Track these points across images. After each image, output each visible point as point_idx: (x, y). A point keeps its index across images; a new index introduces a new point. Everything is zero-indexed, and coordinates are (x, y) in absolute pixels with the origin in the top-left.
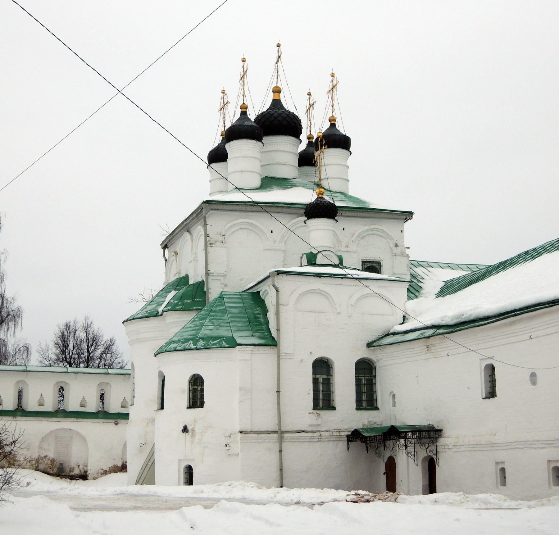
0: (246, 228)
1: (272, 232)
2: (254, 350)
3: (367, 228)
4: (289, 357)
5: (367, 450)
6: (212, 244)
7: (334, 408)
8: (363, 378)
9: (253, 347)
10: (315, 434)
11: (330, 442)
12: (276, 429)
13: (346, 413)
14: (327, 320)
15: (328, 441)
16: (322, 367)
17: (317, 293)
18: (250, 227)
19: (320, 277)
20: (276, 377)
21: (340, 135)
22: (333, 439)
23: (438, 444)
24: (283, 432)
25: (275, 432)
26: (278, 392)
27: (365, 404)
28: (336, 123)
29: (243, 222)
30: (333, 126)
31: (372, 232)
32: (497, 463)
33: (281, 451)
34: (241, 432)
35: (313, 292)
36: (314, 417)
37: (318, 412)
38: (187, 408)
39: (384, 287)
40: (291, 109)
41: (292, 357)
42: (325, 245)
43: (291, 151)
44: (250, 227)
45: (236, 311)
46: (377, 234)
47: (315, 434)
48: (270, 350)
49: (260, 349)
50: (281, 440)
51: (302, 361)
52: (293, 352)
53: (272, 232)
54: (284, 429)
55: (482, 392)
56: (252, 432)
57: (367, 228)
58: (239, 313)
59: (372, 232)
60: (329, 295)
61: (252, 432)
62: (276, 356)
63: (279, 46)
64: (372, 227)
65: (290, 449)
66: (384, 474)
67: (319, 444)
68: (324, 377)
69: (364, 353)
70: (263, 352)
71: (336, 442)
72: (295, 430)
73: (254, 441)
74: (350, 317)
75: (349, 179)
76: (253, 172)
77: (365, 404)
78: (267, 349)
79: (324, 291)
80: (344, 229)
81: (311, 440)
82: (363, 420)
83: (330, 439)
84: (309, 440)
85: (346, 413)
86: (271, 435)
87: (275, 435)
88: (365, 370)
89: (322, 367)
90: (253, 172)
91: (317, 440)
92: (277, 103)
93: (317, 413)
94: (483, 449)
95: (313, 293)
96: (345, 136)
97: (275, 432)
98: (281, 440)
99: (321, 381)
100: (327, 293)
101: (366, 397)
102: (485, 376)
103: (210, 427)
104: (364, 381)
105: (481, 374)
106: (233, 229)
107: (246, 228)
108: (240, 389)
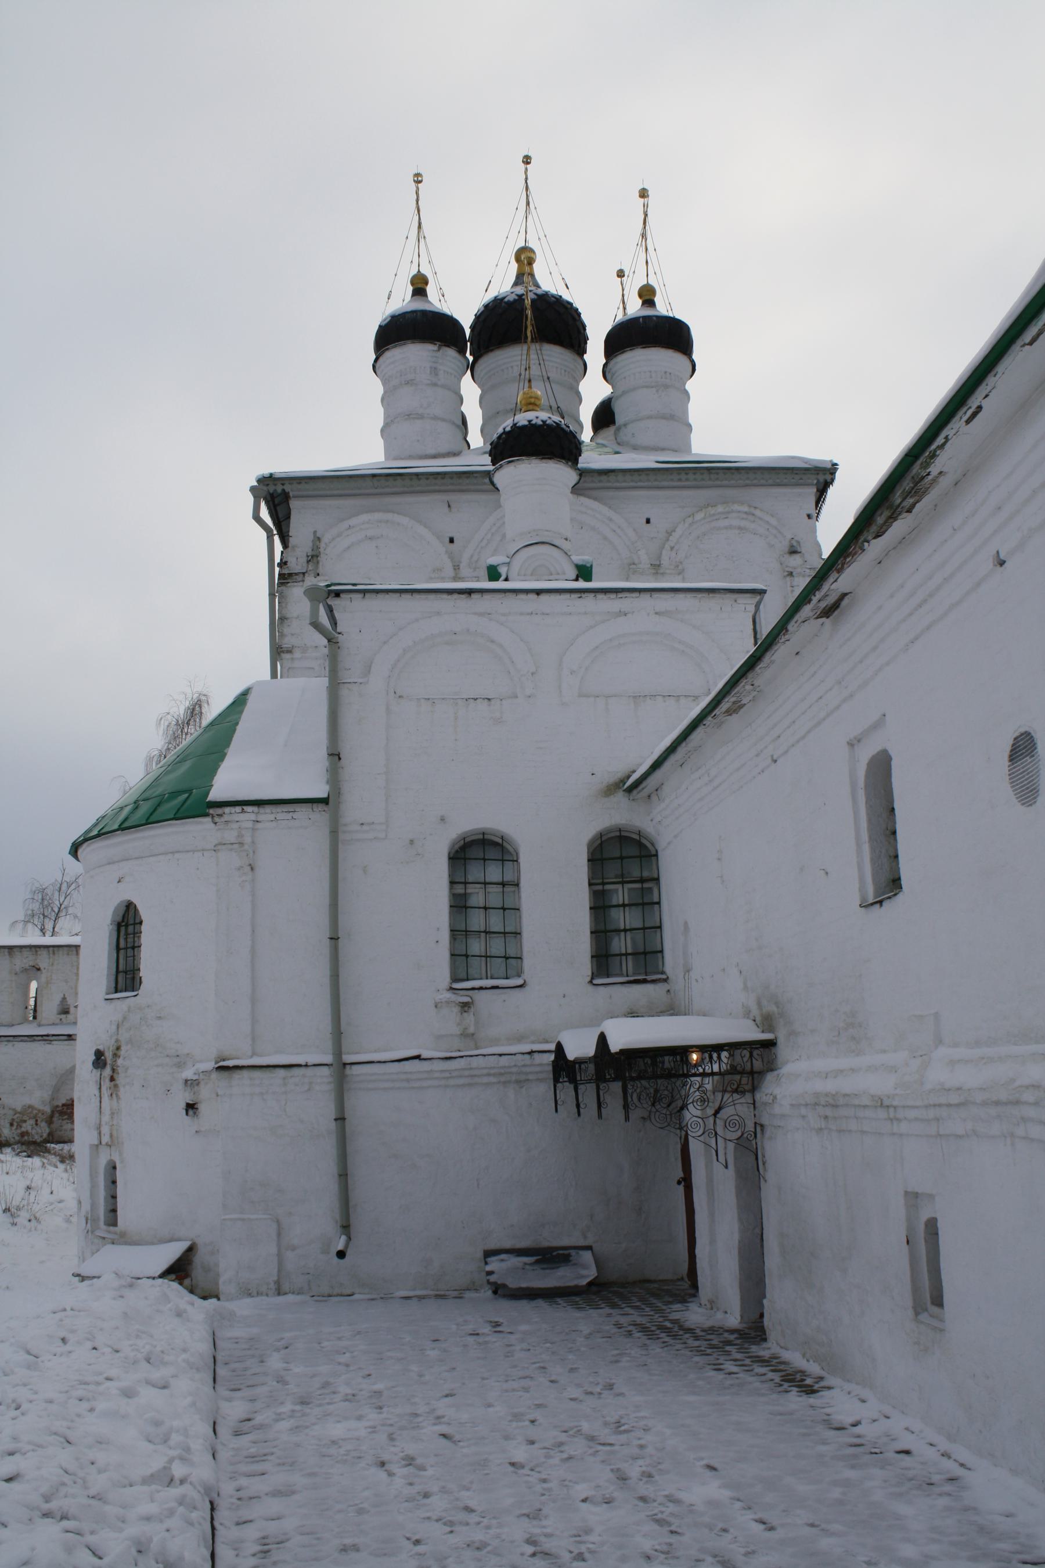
2: (260, 818)
8: (619, 886)
9: (255, 809)
28: (656, 300)
62: (326, 831)
66: (679, 1183)
88: (623, 865)
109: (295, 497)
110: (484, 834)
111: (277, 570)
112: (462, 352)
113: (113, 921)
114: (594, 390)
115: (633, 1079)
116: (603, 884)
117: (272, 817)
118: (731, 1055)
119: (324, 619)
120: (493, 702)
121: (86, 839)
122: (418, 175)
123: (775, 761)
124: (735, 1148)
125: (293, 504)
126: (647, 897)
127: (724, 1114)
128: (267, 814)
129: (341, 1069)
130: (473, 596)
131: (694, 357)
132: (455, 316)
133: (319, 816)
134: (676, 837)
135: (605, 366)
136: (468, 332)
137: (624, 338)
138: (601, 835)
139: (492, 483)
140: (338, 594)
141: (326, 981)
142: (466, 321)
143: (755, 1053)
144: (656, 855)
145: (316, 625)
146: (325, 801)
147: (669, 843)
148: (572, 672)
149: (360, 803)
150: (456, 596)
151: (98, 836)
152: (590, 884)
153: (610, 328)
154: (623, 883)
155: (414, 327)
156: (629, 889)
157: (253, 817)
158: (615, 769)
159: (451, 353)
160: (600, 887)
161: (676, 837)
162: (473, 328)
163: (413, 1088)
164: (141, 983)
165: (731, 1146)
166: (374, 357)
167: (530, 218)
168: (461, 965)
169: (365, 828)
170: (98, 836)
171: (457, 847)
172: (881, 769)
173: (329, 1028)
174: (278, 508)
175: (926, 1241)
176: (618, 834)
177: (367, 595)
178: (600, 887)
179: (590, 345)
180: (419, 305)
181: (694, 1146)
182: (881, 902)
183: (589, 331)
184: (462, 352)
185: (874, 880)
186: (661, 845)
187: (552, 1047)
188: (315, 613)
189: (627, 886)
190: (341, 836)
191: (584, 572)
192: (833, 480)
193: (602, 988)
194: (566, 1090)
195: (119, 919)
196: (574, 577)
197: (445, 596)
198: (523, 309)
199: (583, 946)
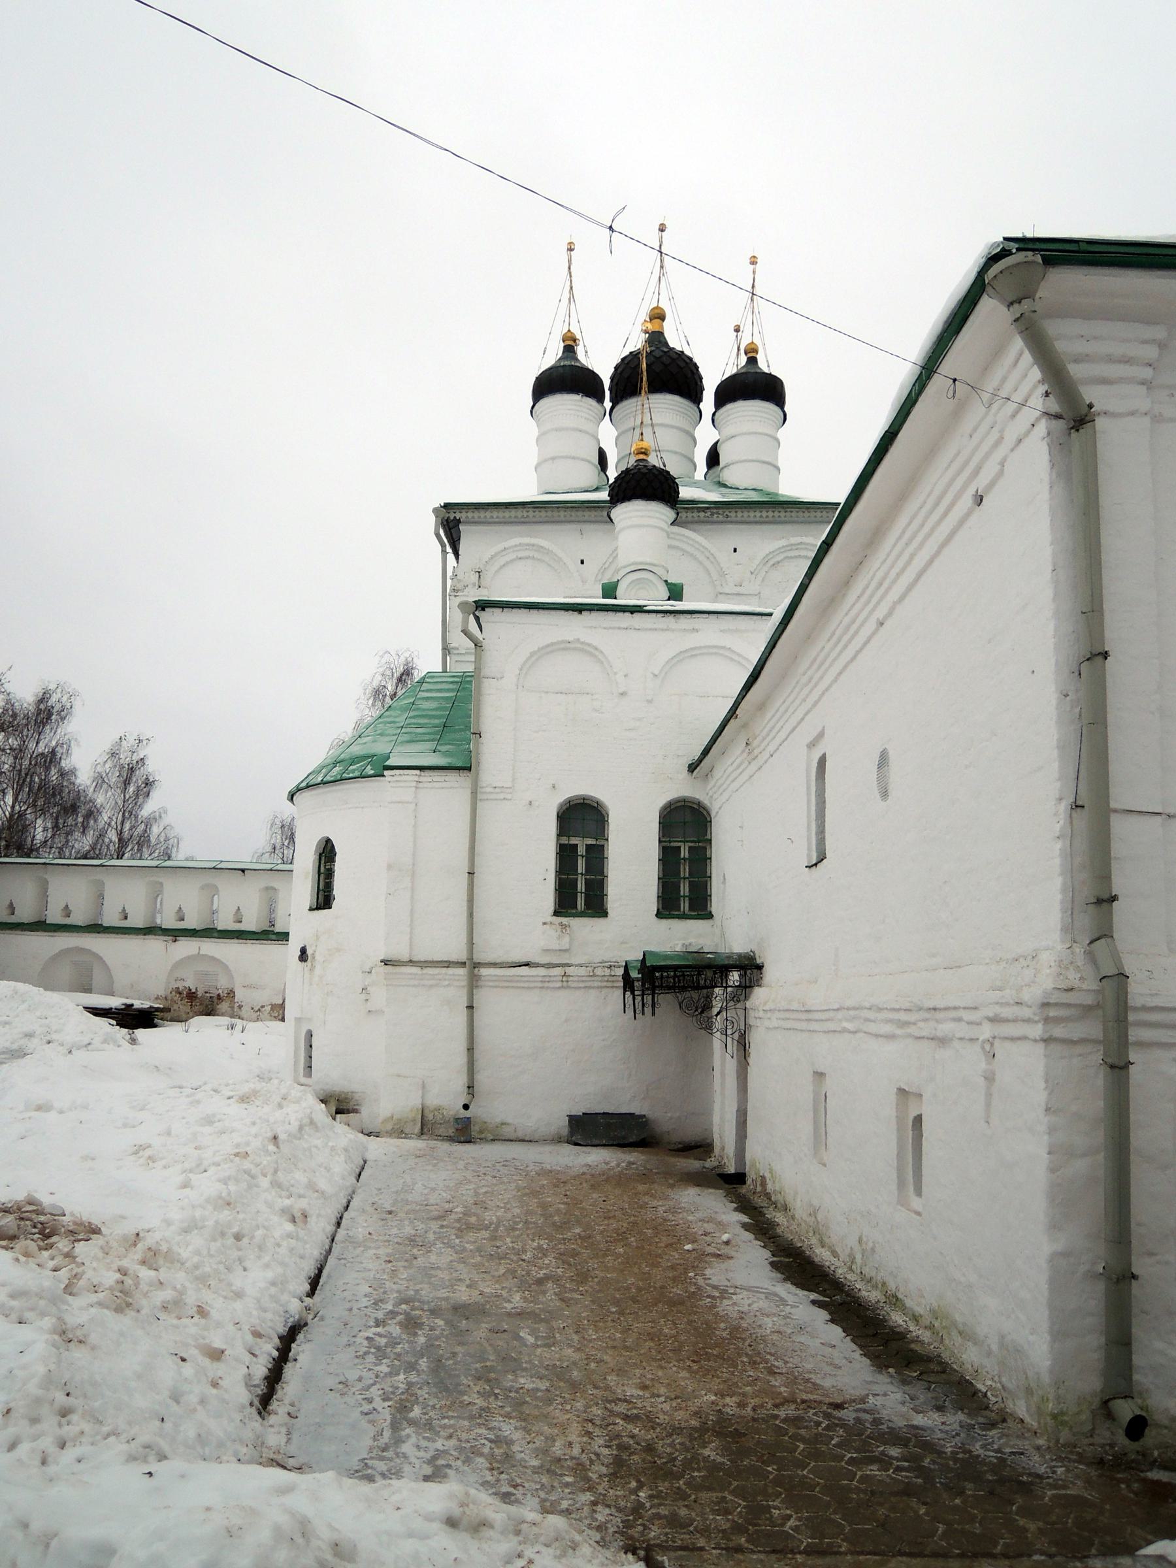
0: (528, 558)
1: (582, 562)
2: (421, 779)
3: (783, 542)
4: (502, 796)
6: (458, 591)
7: (710, 916)
8: (681, 844)
9: (418, 772)
10: (558, 971)
11: (591, 991)
12: (463, 957)
13: (633, 920)
14: (596, 710)
15: (602, 987)
16: (581, 821)
17: (575, 649)
18: (536, 555)
19: (580, 612)
20: (467, 840)
22: (596, 984)
23: (748, 1004)
24: (476, 965)
25: (463, 964)
27: (685, 906)
28: (758, 357)
29: (528, 545)
30: (752, 361)
31: (796, 553)
33: (470, 1007)
34: (386, 962)
35: (565, 646)
37: (565, 920)
38: (311, 909)
39: (737, 631)
40: (679, 348)
41: (509, 796)
42: (640, 559)
43: (678, 425)
44: (536, 555)
45: (434, 705)
47: (558, 971)
48: (458, 778)
50: (474, 982)
52: (509, 784)
53: (582, 562)
54: (478, 957)
55: (809, 849)
56: (411, 962)
57: (783, 542)
58: (436, 709)
59: (796, 553)
61: (411, 962)
62: (469, 792)
63: (662, 229)
64: (794, 540)
67: (562, 993)
69: (681, 787)
70: (444, 785)
71: (605, 991)
72: (510, 960)
73: (416, 982)
74: (650, 702)
75: (780, 465)
76: (574, 458)
77: (685, 906)
78: (452, 778)
79: (589, 645)
80: (735, 550)
81: (544, 985)
82: (679, 938)
83: (587, 984)
84: (540, 985)
85: (633, 920)
86: (451, 971)
87: (462, 971)
88: (686, 831)
89: (581, 821)
90: (574, 458)
91: (559, 984)
92: (656, 338)
93: (561, 924)
94: (798, 1025)
95: (564, 649)
97: (463, 964)
98: (474, 982)
99: (581, 850)
101: (685, 883)
103: (338, 950)
105: (808, 794)
106: (502, 561)
107: (528, 558)
108: (390, 867)
109: (468, 523)
111: (449, 582)
112: (600, 399)
114: (706, 435)
121: (299, 789)
126: (701, 859)
132: (696, 360)
135: (714, 414)
136: (607, 383)
137: (730, 392)
145: (465, 632)
151: (308, 786)
155: (565, 379)
157: (416, 778)
159: (591, 402)
170: (308, 786)
173: (465, 941)
184: (600, 399)
188: (465, 622)
190: (479, 796)
191: (675, 592)
198: (639, 365)
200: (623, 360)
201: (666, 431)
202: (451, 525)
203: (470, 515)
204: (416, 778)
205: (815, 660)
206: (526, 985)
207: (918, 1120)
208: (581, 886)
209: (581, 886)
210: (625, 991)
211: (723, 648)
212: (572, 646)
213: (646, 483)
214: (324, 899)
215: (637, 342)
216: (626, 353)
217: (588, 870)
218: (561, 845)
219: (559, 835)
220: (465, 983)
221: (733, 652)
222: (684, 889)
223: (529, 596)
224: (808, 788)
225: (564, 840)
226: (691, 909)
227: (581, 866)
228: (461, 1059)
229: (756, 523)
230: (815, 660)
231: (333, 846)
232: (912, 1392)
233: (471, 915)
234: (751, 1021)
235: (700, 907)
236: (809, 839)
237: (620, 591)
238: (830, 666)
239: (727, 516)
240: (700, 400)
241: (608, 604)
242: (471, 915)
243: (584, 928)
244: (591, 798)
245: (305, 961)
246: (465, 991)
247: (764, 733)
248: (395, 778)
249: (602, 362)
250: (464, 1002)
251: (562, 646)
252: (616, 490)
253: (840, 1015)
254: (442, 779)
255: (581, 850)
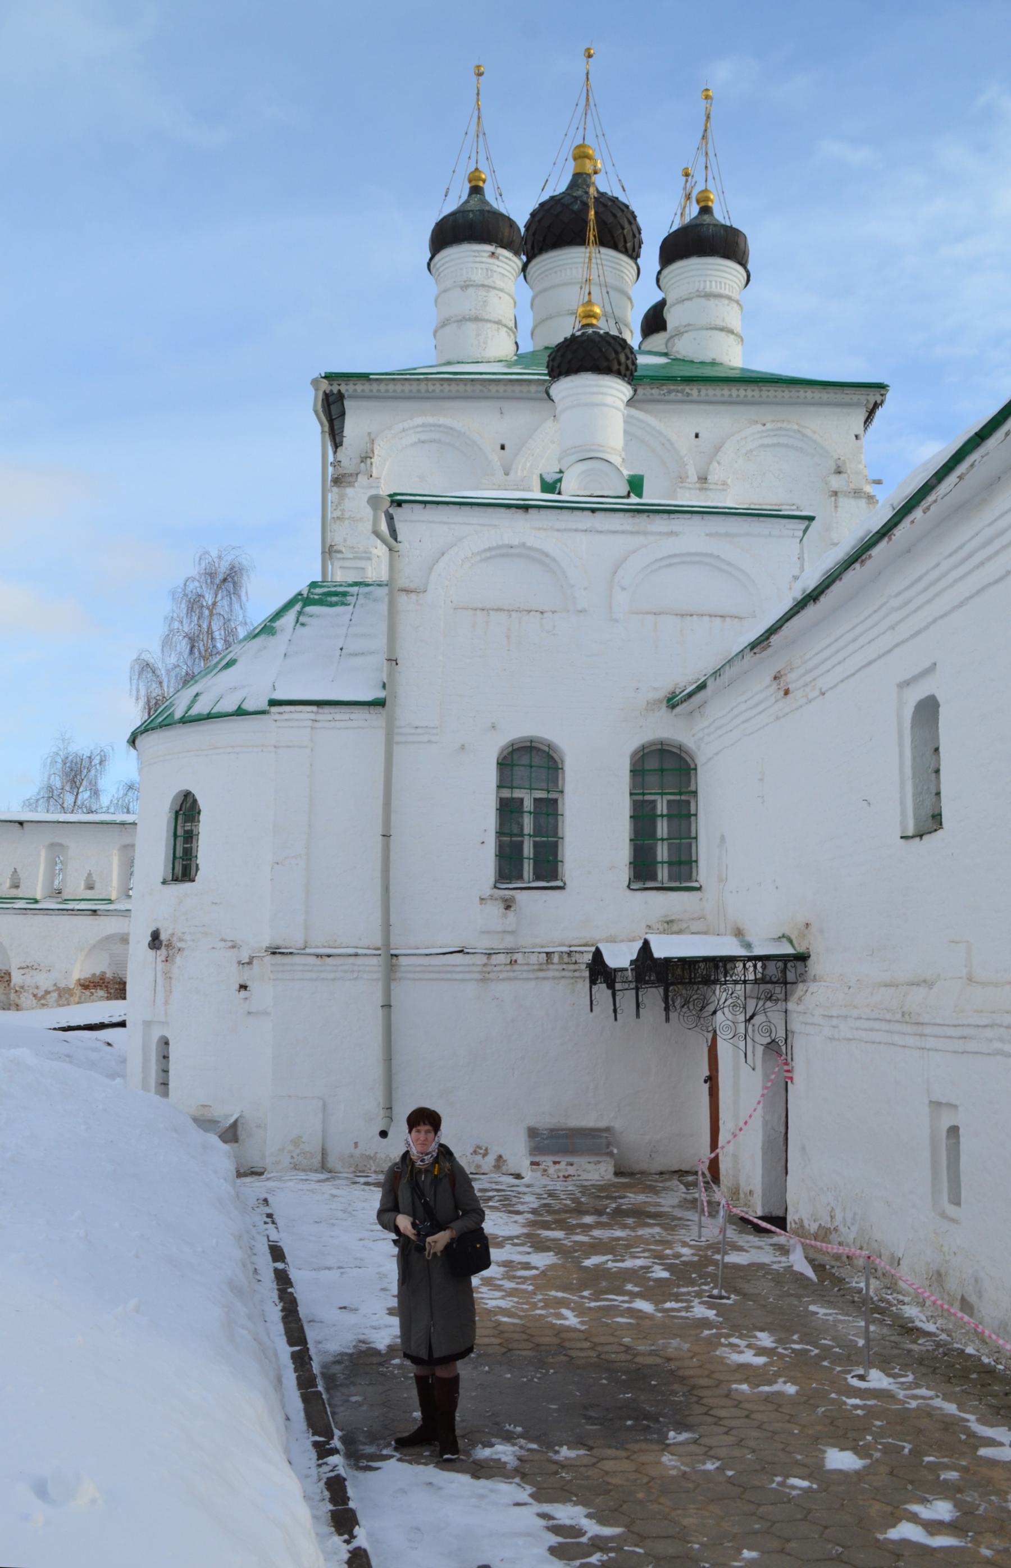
2: (319, 717)
4: (425, 738)
5: (667, 1009)
8: (658, 798)
9: (314, 708)
11: (563, 982)
16: (529, 772)
17: (519, 555)
21: (715, 225)
23: (791, 1006)
26: (386, 836)
27: (663, 873)
29: (434, 425)
32: (936, 1105)
33: (387, 1006)
36: (496, 909)
38: (164, 883)
39: (727, 535)
41: (434, 739)
46: (787, 446)
49: (337, 717)
51: (463, 747)
55: (903, 814)
60: (554, 560)
65: (420, 999)
66: (706, 1081)
68: (540, 794)
88: (664, 779)
89: (529, 772)
96: (731, 227)
99: (528, 805)
100: (547, 555)
101: (663, 843)
102: (915, 748)
104: (662, 807)
105: (901, 744)
109: (355, 397)
110: (531, 741)
113: (171, 809)
114: (644, 296)
115: (672, 984)
116: (644, 794)
117: (330, 717)
118: (764, 967)
119: (384, 527)
120: (545, 615)
122: (478, 67)
123: (824, 694)
124: (764, 1053)
125: (347, 404)
126: (683, 814)
127: (757, 1020)
128: (327, 712)
129: (392, 959)
130: (530, 510)
131: (749, 267)
133: (375, 719)
134: (717, 754)
135: (659, 273)
137: (681, 246)
138: (643, 747)
139: (548, 394)
140: (399, 504)
141: (378, 875)
142: (521, 219)
143: (789, 965)
144: (695, 769)
145: (377, 533)
146: (379, 703)
147: (710, 759)
148: (623, 589)
149: (413, 705)
150: (513, 510)
152: (631, 794)
153: (666, 234)
154: (662, 794)
155: (468, 226)
156: (669, 802)
157: (312, 716)
158: (665, 685)
160: (640, 798)
161: (717, 754)
162: (528, 227)
163: (456, 980)
164: (197, 869)
165: (760, 1050)
166: (429, 256)
167: (589, 112)
168: (509, 866)
169: (419, 731)
171: (505, 753)
172: (928, 711)
174: (332, 407)
175: (947, 1150)
176: (659, 747)
177: (428, 506)
178: (640, 798)
179: (644, 250)
180: (474, 204)
181: (722, 1047)
182: (921, 836)
183: (644, 236)
185: (915, 815)
186: (700, 760)
187: (593, 949)
189: (666, 798)
190: (397, 738)
191: (636, 485)
192: (882, 402)
193: (639, 893)
194: (602, 990)
195: (178, 808)
196: (625, 493)
197: (503, 510)
199: (622, 853)
200: (542, 205)
201: (619, 290)
202: (331, 399)
203: (359, 388)
204: (312, 716)
205: (920, 579)
206: (460, 976)
207: (954, 1131)
208: (528, 850)
209: (528, 850)
210: (593, 982)
211: (711, 555)
212: (513, 551)
213: (587, 353)
214: (183, 868)
215: (559, 186)
216: (545, 197)
217: (537, 831)
218: (501, 799)
219: (499, 787)
220: (379, 976)
221: (723, 560)
222: (662, 852)
223: (477, 488)
224: (901, 738)
225: (506, 794)
226: (671, 878)
227: (528, 824)
228: (375, 1072)
229: (724, 403)
230: (920, 579)
231: (195, 801)
232: (349, 1319)
233: (386, 889)
234: (795, 1025)
235: (683, 872)
236: (902, 803)
237: (564, 486)
238: (951, 586)
239: (688, 395)
240: (638, 256)
241: (551, 498)
242: (386, 889)
243: (534, 902)
244: (541, 741)
245: (159, 948)
246: (380, 985)
247: (811, 664)
248: (285, 716)
249: (519, 208)
250: (379, 999)
251: (504, 551)
252: (558, 360)
253: (989, 1033)
254: (346, 717)
255: (528, 805)
